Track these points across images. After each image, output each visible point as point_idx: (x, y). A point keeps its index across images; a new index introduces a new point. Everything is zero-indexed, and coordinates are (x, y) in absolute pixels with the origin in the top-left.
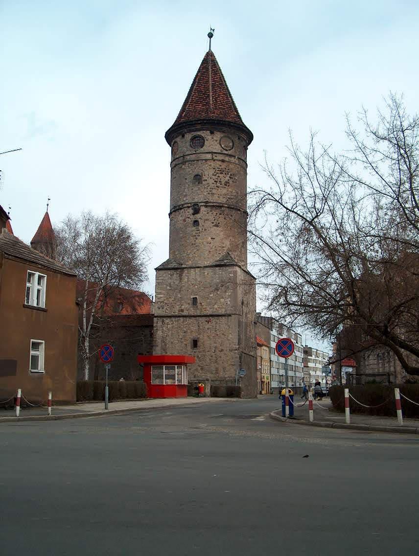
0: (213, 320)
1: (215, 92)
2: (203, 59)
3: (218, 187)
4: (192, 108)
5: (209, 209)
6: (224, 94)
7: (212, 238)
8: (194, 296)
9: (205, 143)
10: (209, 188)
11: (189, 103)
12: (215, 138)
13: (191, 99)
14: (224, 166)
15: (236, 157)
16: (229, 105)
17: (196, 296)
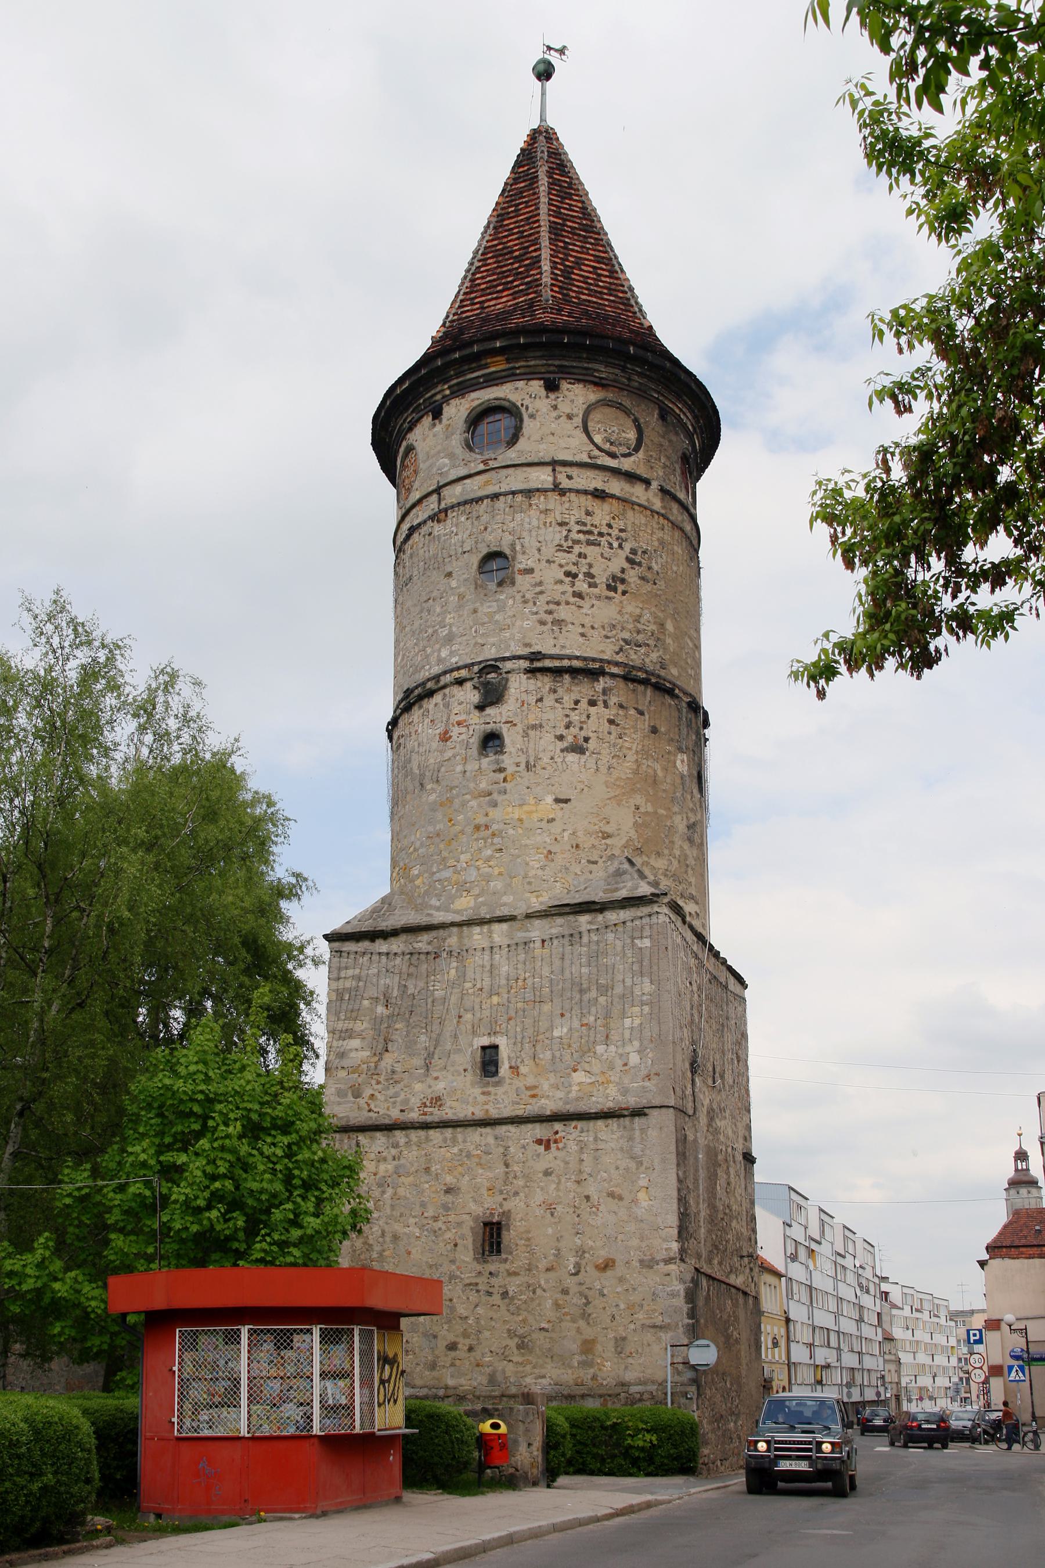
0: (571, 1134)
3: (579, 595)
5: (545, 682)
8: (486, 1041)
10: (543, 599)
12: (565, 408)
14: (602, 513)
15: (655, 485)
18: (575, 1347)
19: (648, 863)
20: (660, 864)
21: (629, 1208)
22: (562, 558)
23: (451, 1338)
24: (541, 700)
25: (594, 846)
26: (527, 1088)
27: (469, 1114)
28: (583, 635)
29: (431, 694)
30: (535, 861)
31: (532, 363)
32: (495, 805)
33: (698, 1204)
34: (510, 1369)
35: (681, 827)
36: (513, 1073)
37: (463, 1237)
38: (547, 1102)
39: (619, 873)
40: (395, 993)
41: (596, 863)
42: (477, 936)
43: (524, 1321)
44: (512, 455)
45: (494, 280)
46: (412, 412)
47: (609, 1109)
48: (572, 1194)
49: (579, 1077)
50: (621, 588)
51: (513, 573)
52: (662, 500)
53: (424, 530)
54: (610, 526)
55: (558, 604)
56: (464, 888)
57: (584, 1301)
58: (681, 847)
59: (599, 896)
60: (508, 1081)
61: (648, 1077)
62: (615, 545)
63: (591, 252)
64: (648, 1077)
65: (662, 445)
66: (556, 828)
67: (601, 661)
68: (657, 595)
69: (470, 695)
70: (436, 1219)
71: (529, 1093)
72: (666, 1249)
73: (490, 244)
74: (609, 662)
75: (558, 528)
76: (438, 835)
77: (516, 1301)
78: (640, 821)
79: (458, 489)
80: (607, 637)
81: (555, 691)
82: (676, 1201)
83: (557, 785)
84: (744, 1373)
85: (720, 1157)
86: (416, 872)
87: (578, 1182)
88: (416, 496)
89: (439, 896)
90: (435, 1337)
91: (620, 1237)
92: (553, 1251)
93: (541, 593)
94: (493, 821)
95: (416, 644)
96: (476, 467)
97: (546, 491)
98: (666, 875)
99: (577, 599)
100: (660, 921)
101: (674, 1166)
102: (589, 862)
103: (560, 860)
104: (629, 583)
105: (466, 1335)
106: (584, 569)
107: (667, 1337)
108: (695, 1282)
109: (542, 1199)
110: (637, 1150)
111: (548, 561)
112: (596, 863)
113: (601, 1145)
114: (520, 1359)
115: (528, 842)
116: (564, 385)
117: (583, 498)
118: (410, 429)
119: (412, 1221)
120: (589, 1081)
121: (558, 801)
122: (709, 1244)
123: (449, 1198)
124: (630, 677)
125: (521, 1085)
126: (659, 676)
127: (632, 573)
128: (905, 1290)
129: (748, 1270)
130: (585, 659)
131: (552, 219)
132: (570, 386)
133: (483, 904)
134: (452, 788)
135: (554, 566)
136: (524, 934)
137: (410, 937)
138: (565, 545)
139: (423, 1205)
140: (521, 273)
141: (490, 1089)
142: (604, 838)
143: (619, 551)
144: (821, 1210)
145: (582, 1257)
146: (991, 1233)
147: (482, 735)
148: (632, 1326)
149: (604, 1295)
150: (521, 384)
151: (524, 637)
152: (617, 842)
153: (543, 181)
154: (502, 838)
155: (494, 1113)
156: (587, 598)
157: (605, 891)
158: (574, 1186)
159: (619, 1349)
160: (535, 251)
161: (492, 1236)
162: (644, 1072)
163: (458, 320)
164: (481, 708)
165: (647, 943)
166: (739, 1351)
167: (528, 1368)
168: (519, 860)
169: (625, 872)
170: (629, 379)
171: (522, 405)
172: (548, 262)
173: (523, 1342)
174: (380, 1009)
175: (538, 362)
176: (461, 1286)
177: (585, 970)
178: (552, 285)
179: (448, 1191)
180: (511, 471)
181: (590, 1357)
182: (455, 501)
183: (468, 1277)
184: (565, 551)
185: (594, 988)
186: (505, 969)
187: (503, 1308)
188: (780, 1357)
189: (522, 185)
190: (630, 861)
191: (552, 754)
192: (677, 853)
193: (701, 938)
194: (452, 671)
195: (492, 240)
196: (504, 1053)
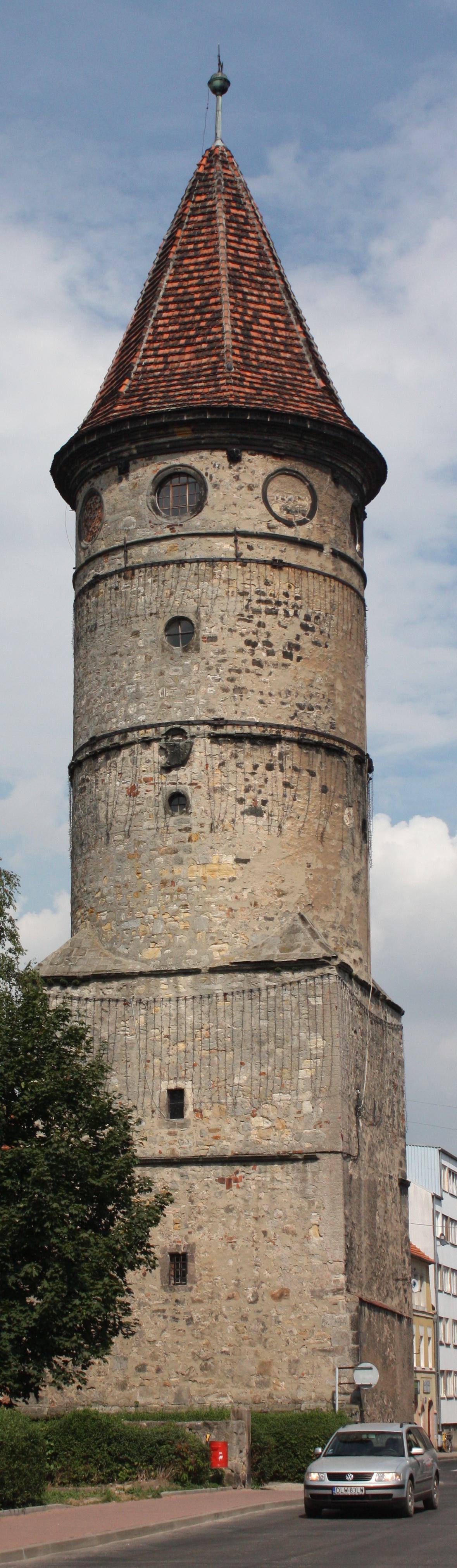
0: (253, 1175)
1: (241, 304)
2: (190, 175)
3: (258, 663)
4: (154, 364)
5: (226, 750)
6: (275, 310)
7: (238, 861)
8: (173, 1086)
9: (209, 500)
10: (226, 666)
11: (144, 346)
12: (246, 479)
13: (150, 330)
14: (280, 582)
15: (327, 549)
16: (296, 350)
17: (180, 1084)
18: (253, 1369)
19: (317, 918)
20: (328, 917)
22: (243, 627)
23: (140, 1359)
25: (270, 904)
26: (211, 1131)
27: (157, 1153)
28: (261, 702)
30: (218, 917)
31: (216, 434)
32: (180, 862)
33: (360, 1236)
35: (346, 876)
36: (197, 1116)
38: (229, 1143)
39: (293, 931)
41: (271, 919)
42: (164, 985)
43: (207, 1345)
44: (196, 523)
45: (176, 331)
46: (99, 461)
47: (284, 1152)
48: (251, 1229)
49: (258, 1121)
50: (296, 654)
51: (198, 639)
52: (334, 563)
53: (111, 583)
54: (286, 595)
55: (239, 671)
56: (151, 939)
57: (261, 1327)
58: (347, 898)
59: (275, 954)
60: (193, 1123)
61: (319, 1124)
62: (291, 612)
63: (268, 301)
64: (319, 1124)
65: (334, 508)
66: (236, 887)
67: (278, 726)
68: (328, 657)
71: (211, 1135)
72: (335, 1281)
73: (170, 285)
74: (285, 728)
75: (240, 598)
76: (126, 885)
77: (200, 1326)
78: (311, 878)
79: (145, 550)
80: (283, 703)
81: (236, 757)
82: (343, 1237)
83: (237, 845)
84: (399, 1391)
85: (379, 1188)
86: (104, 918)
87: (256, 1219)
89: (126, 945)
90: (126, 1359)
91: (294, 1269)
92: (233, 1281)
93: (224, 660)
94: (178, 877)
95: (102, 694)
96: (162, 531)
97: (227, 561)
98: (334, 927)
99: (256, 667)
100: (331, 981)
101: (342, 1206)
102: (266, 919)
103: (241, 917)
104: (304, 649)
106: (263, 638)
107: (335, 1360)
108: (359, 1311)
109: (224, 1233)
110: (310, 1191)
111: (230, 630)
112: (271, 919)
113: (277, 1185)
114: (203, 1380)
115: (211, 899)
116: (246, 456)
117: (262, 568)
120: (268, 1126)
121: (238, 861)
122: (369, 1273)
124: (308, 742)
129: (402, 1292)
130: (264, 725)
131: (231, 265)
132: (251, 457)
133: (170, 956)
134: (140, 843)
135: (236, 635)
136: (208, 987)
137: (100, 985)
138: (246, 614)
140: (202, 328)
142: (279, 896)
143: (295, 619)
145: (259, 1287)
147: (168, 795)
148: (304, 1350)
149: (279, 1322)
150: (205, 454)
151: (208, 703)
153: (222, 218)
154: (188, 894)
155: (180, 1153)
156: (265, 666)
157: (282, 950)
158: (253, 1223)
159: (293, 1370)
160: (216, 304)
162: (315, 1120)
163: (143, 372)
165: (319, 1001)
167: (211, 1388)
168: (203, 916)
170: (305, 449)
171: (207, 474)
172: (229, 321)
173: (206, 1364)
175: (222, 434)
176: (149, 1312)
177: (264, 1023)
178: (234, 347)
180: (195, 539)
181: (267, 1377)
182: (141, 561)
183: (156, 1304)
184: (245, 620)
185: (272, 1040)
186: (190, 1018)
187: (188, 1332)
188: (426, 1364)
189: (200, 218)
191: (233, 816)
192: (344, 904)
194: (138, 728)
195: (173, 281)
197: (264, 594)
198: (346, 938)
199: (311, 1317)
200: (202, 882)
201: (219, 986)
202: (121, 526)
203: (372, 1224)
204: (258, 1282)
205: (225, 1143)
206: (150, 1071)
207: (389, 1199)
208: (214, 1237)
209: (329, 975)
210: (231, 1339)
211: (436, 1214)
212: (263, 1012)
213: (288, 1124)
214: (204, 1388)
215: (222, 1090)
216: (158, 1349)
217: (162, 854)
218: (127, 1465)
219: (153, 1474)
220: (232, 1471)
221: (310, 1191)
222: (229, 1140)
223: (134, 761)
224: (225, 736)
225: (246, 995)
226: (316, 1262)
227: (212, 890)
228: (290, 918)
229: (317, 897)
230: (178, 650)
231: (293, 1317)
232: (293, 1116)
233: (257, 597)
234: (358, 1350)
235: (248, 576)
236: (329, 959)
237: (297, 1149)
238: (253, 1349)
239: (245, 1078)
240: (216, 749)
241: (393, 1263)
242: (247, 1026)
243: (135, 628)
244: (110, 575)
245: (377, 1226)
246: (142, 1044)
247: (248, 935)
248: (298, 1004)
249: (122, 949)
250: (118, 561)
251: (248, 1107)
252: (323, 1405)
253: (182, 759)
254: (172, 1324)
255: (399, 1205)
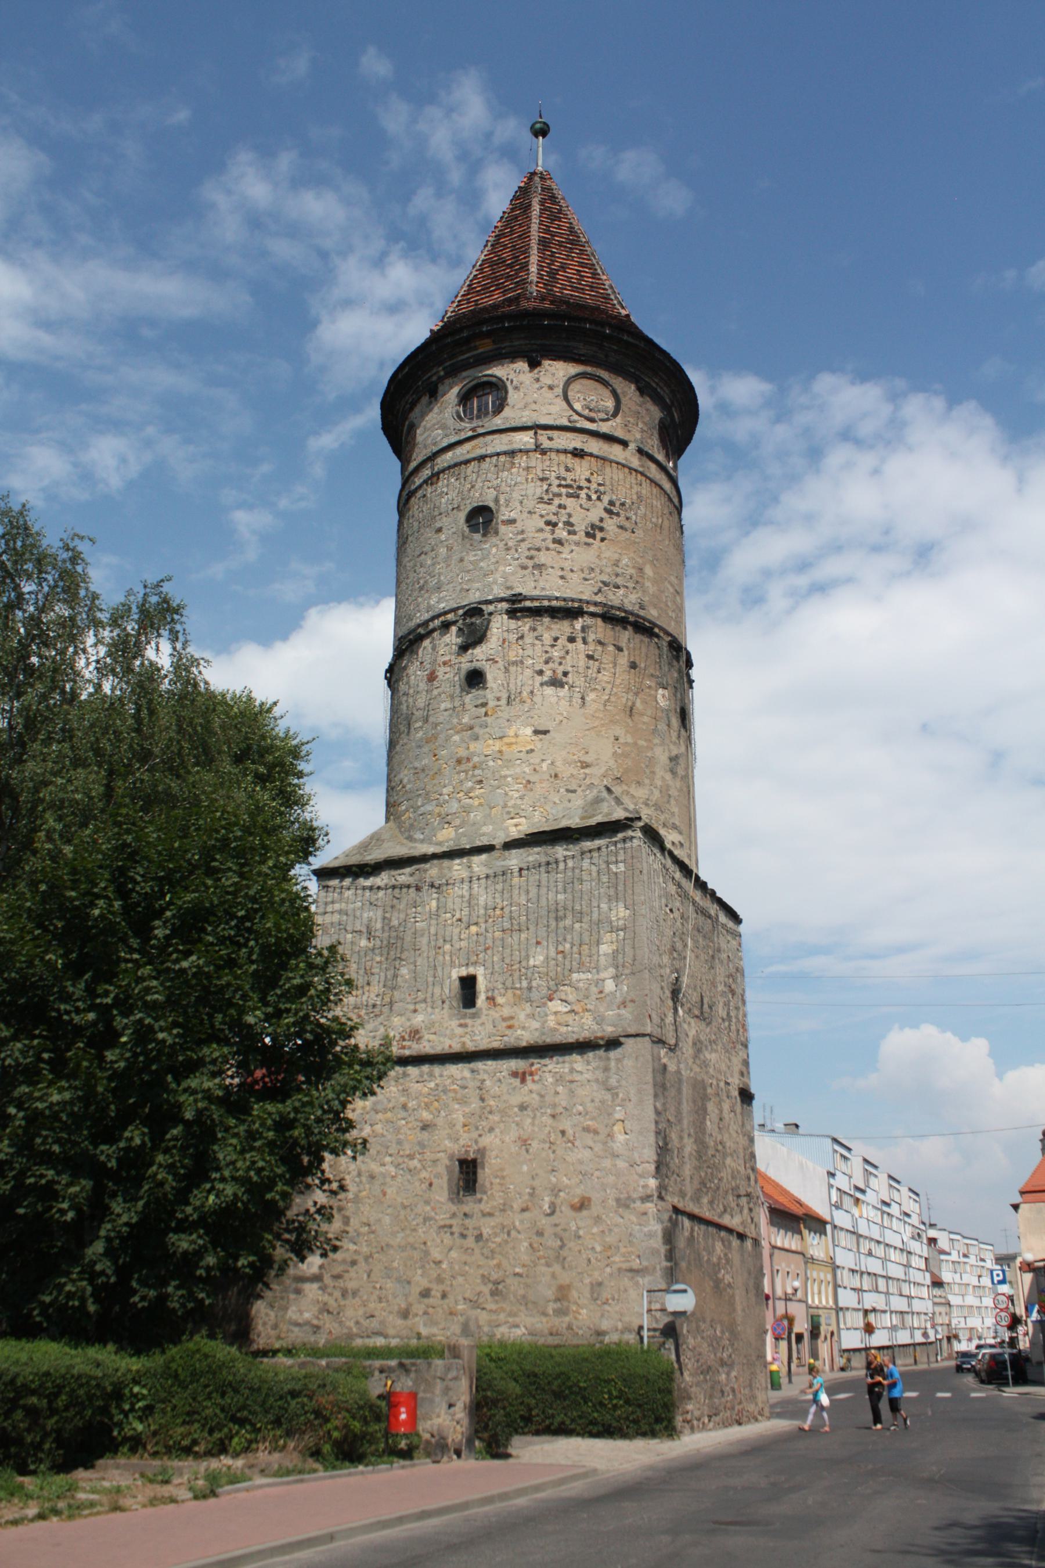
0: (552, 1067)
3: (559, 542)
5: (525, 625)
7: (536, 732)
8: (464, 972)
9: (510, 400)
10: (524, 545)
12: (547, 380)
14: (581, 470)
15: (632, 446)
17: (471, 970)
18: (550, 1293)
19: (628, 793)
20: (641, 793)
21: (605, 1143)
23: (424, 1283)
24: (522, 637)
26: (504, 1019)
28: (562, 577)
29: (421, 638)
30: (514, 792)
31: (516, 343)
32: (476, 738)
33: (681, 1138)
34: (483, 1317)
35: (662, 756)
37: (438, 1176)
39: (597, 801)
40: (379, 925)
41: (574, 791)
42: (457, 867)
43: (499, 1266)
44: (498, 422)
48: (548, 1129)
49: (556, 1005)
50: (599, 535)
54: (589, 481)
55: (539, 550)
56: (446, 820)
57: (559, 1243)
60: (485, 1012)
61: (624, 1004)
62: (594, 497)
64: (624, 1004)
66: (535, 759)
67: (580, 601)
69: (453, 638)
70: (411, 1157)
71: (504, 1024)
74: (588, 603)
75: (539, 483)
76: (423, 770)
78: (619, 751)
79: (450, 454)
80: (586, 579)
81: (534, 630)
84: (739, 1320)
85: (709, 1090)
87: (553, 1116)
88: (413, 465)
89: (422, 830)
90: (409, 1283)
91: (597, 1173)
93: (523, 540)
94: (473, 754)
97: (527, 452)
98: (647, 805)
102: (568, 791)
103: (539, 789)
105: (440, 1280)
106: (564, 519)
107: (645, 1281)
108: (674, 1223)
110: (613, 1082)
111: (530, 512)
112: (574, 791)
113: (576, 1077)
114: (493, 1307)
115: (508, 773)
117: (562, 457)
118: (411, 409)
119: (388, 1159)
120: (566, 1010)
121: (536, 732)
122: (696, 1182)
123: (425, 1135)
124: (612, 618)
125: (497, 1016)
126: (638, 616)
127: (610, 521)
128: (953, 1236)
129: (746, 1211)
130: (565, 600)
133: (464, 834)
134: (437, 725)
135: (536, 517)
138: (546, 497)
139: (399, 1142)
141: (469, 1021)
142: (583, 768)
143: (598, 503)
144: (866, 1161)
145: (556, 1196)
146: (1022, 1180)
148: (608, 1270)
149: (579, 1237)
152: (596, 771)
155: (471, 1047)
158: (550, 1121)
161: (468, 1173)
164: (464, 648)
166: (733, 1296)
167: (502, 1317)
169: (602, 800)
174: (364, 943)
176: (435, 1227)
179: (425, 1127)
181: (565, 1304)
183: (442, 1218)
185: (569, 915)
186: (482, 901)
187: (477, 1251)
190: (609, 790)
193: (686, 870)
196: (481, 984)
197: (565, 479)
198: (662, 818)
199: (616, 1230)
200: (498, 755)
201: (514, 862)
202: (429, 441)
203: (700, 1127)
204: (555, 1191)
205: (519, 1032)
206: (441, 958)
207: (726, 1106)
208: (507, 1139)
209: (632, 838)
210: (525, 1258)
211: (831, 1186)
212: (560, 886)
213: (589, 1007)
214: (494, 1317)
215: (516, 974)
216: (444, 1271)
217: (458, 732)
218: (248, 1427)
219: (282, 1442)
220: (433, 1436)
221: (613, 1082)
222: (524, 1028)
223: (434, 648)
224: (521, 610)
225: (543, 869)
226: (621, 1164)
227: (509, 763)
228: (595, 791)
229: (626, 771)
230: (477, 537)
231: (595, 1230)
232: (594, 997)
233: (557, 482)
234: (671, 1268)
235: (548, 463)
236: (631, 820)
237: (599, 1034)
238: (551, 1270)
239: (541, 958)
240: (513, 624)
241: (733, 1178)
242: (543, 902)
243: (438, 525)
244: (420, 486)
245: (708, 1132)
246: (433, 931)
247: (547, 808)
248: (598, 872)
249: (419, 836)
250: (426, 473)
251: (545, 991)
252: (631, 1338)
253: (479, 634)
254: (459, 1241)
255: (739, 1117)
